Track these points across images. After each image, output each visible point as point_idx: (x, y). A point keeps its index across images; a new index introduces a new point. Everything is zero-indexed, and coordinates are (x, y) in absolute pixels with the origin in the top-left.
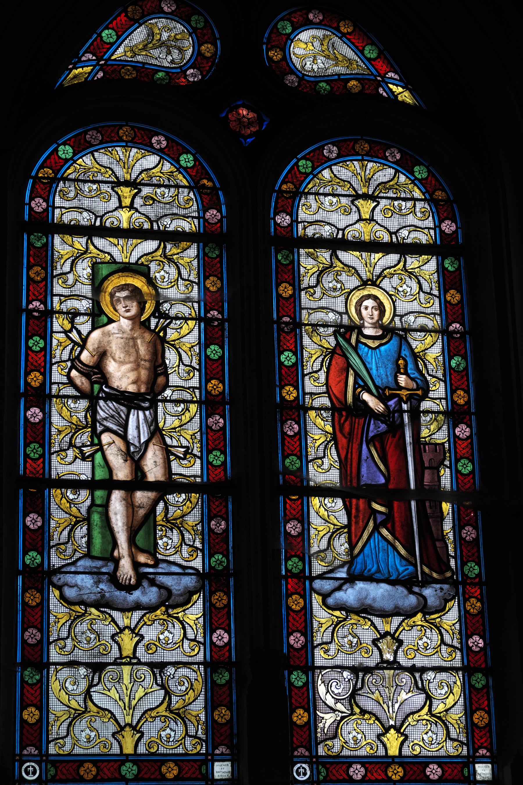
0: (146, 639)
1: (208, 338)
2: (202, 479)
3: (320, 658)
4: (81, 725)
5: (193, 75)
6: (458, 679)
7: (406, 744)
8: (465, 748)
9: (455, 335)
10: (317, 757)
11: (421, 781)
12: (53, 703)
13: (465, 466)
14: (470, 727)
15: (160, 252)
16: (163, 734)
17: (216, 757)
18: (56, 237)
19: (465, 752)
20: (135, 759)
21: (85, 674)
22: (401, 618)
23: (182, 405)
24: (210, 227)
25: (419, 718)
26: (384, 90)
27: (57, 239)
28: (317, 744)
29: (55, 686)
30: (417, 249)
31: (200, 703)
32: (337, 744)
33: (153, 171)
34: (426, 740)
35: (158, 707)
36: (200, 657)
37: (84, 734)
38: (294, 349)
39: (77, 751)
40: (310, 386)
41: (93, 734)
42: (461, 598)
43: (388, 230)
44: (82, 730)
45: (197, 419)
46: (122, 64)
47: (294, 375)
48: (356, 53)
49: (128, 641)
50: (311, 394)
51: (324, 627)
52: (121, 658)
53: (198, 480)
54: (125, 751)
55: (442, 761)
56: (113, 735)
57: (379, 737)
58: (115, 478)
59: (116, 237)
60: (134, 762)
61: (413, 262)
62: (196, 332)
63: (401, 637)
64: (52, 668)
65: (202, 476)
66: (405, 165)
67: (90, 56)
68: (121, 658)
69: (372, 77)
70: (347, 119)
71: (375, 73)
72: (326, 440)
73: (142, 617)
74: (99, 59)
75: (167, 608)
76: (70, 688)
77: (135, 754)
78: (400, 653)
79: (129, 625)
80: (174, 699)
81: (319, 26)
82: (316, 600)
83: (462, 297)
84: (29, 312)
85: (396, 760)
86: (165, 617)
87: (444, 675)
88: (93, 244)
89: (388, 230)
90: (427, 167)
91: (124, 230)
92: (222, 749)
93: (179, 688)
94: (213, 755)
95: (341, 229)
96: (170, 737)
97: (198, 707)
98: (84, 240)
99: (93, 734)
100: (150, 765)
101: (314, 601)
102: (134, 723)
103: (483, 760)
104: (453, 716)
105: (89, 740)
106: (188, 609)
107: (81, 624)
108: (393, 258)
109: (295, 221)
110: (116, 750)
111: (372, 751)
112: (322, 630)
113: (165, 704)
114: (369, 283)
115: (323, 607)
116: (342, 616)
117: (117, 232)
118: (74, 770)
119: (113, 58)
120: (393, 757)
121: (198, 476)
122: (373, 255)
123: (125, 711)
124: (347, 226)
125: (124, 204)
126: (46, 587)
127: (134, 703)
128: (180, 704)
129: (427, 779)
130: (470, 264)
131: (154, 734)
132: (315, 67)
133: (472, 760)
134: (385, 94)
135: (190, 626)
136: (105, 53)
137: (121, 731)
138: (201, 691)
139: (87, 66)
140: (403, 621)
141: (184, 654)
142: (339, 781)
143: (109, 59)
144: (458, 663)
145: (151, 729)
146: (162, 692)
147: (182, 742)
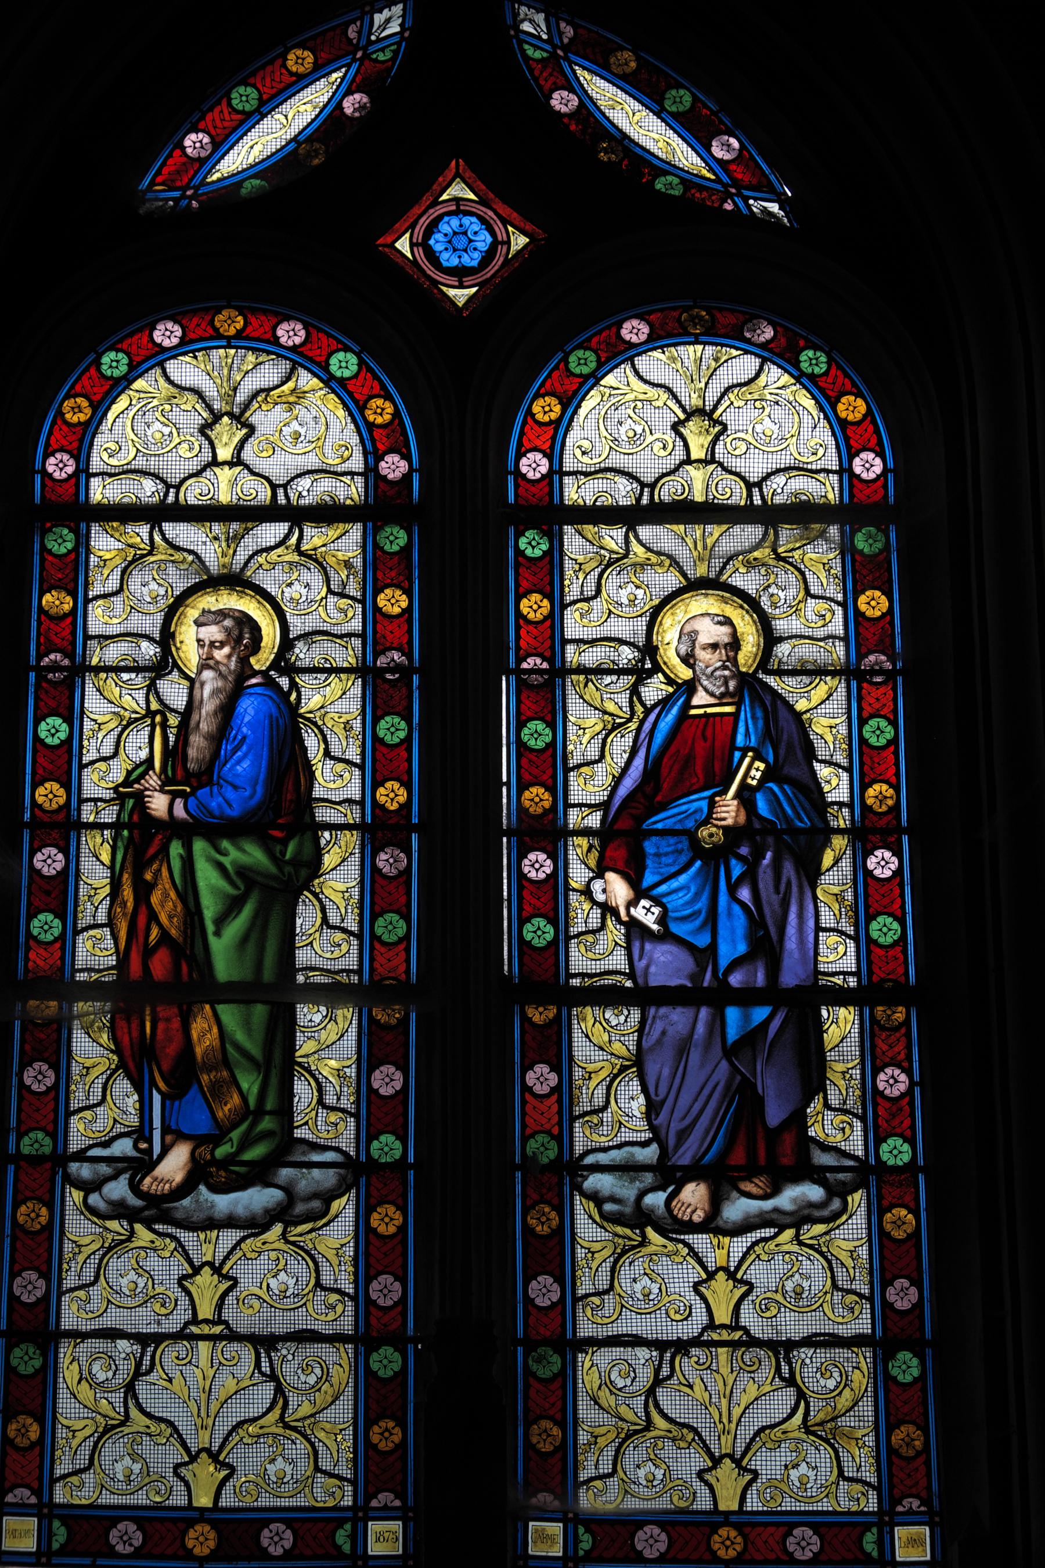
2: (859, 981)
3: (72, 1315)
6: (864, 1358)
7: (229, 1485)
8: (873, 1496)
9: (389, 676)
10: (52, 1505)
11: (174, 1557)
12: (65, 1405)
13: (46, 927)
14: (888, 1458)
16: (794, 1474)
17: (371, 1514)
18: (568, 529)
19: (348, 1501)
22: (239, 1234)
25: (261, 1432)
28: (53, 1481)
29: (69, 1373)
30: (328, 513)
31: (343, 1411)
35: (264, 1414)
39: (107, 1499)
41: (137, 1467)
42: (363, 1191)
43: (743, 479)
49: (722, 1294)
51: (87, 1251)
52: (195, 1321)
54: (722, 1507)
55: (823, 1524)
60: (738, 1527)
61: (314, 537)
66: (782, 353)
68: (195, 1321)
69: (719, 187)
70: (677, 271)
71: (725, 179)
73: (239, 1243)
77: (741, 1511)
78: (746, 1309)
79: (724, 1264)
80: (293, 1400)
84: (40, 670)
85: (207, 1515)
86: (795, 1248)
88: (637, 537)
89: (743, 479)
90: (828, 355)
92: (385, 1498)
93: (822, 1382)
95: (647, 485)
96: (814, 1478)
98: (619, 533)
99: (137, 1467)
100: (238, 1528)
101: (69, 1202)
102: (215, 1447)
105: (128, 1480)
106: (838, 1227)
108: (751, 533)
109: (556, 472)
111: (158, 1499)
112: (81, 1258)
113: (277, 1412)
115: (838, 1222)
118: (778, 1543)
123: (720, 1426)
124: (769, 475)
126: (567, 1189)
127: (214, 1407)
128: (306, 1409)
129: (188, 1555)
130: (922, 537)
131: (778, 1473)
133: (360, 1515)
135: (328, 1260)
137: (714, 1467)
138: (866, 1390)
140: (243, 1239)
142: (766, 1562)
145: (248, 1460)
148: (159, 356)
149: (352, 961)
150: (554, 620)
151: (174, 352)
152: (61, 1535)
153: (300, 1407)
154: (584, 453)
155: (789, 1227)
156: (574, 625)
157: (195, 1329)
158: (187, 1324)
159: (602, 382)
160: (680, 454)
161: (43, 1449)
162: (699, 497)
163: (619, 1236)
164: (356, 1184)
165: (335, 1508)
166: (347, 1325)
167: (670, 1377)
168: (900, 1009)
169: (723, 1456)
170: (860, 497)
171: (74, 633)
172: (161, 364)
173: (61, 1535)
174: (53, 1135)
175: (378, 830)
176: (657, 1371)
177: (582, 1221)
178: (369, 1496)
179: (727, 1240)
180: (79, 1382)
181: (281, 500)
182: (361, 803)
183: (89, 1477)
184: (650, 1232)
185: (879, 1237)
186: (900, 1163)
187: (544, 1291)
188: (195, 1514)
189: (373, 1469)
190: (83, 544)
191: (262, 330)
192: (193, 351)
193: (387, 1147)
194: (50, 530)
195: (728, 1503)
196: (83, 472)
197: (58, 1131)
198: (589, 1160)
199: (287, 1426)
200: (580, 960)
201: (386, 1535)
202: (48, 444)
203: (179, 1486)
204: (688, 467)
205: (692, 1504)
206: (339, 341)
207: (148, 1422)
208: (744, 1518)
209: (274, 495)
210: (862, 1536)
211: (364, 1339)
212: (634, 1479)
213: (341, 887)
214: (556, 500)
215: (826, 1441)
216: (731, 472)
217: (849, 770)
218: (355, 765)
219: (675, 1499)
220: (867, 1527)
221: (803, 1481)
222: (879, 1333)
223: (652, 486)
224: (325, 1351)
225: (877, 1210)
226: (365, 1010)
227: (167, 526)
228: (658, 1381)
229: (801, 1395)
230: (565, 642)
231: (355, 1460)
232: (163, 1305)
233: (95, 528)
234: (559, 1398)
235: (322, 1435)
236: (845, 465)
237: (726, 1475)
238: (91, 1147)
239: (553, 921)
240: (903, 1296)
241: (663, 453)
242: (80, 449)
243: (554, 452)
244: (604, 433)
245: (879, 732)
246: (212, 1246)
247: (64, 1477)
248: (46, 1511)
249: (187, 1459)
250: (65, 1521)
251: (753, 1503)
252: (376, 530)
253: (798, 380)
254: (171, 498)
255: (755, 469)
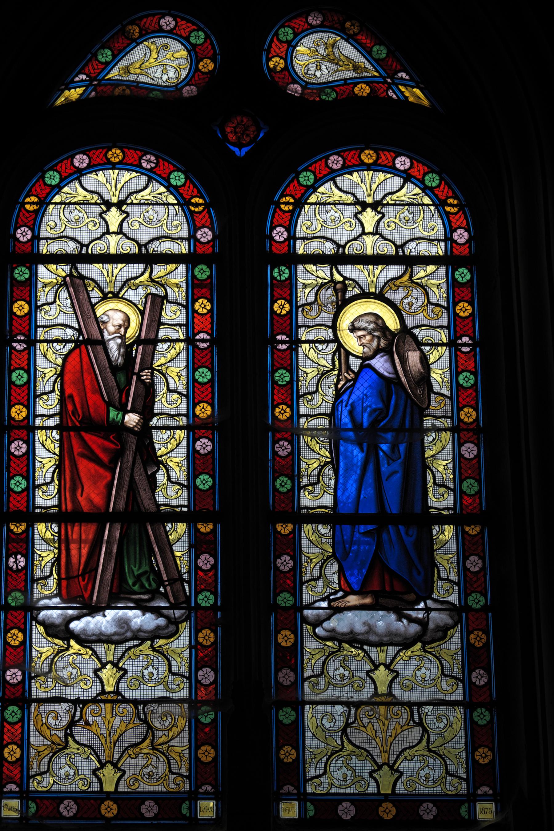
0: (130, 673)
1: (194, 363)
4: (336, 764)
5: (189, 91)
6: (459, 712)
8: (464, 784)
10: (306, 794)
15: (406, 277)
16: (422, 773)
19: (464, 790)
20: (116, 796)
21: (68, 708)
22: (397, 648)
23: (168, 432)
24: (458, 248)
26: (394, 92)
27: (41, 269)
28: (306, 781)
32: (49, 780)
33: (398, 194)
34: (420, 776)
36: (184, 694)
37: (63, 771)
38: (26, 367)
40: (41, 407)
43: (393, 243)
44: (62, 766)
45: (450, 448)
46: (116, 83)
47: (28, 395)
48: (363, 55)
50: (307, 416)
52: (103, 692)
53: (185, 509)
55: (437, 800)
56: (371, 774)
57: (95, 772)
58: (360, 512)
59: (315, 264)
62: (183, 356)
63: (125, 666)
64: (307, 707)
65: (188, 506)
67: (84, 77)
72: (320, 465)
74: (91, 80)
75: (424, 644)
76: (327, 725)
81: (323, 27)
82: (38, 631)
83: (193, 306)
85: (112, 796)
87: (443, 709)
89: (393, 243)
91: (113, 255)
94: (475, 795)
97: (182, 743)
102: (391, 763)
103: (207, 796)
104: (452, 750)
105: (345, 780)
107: (333, 661)
110: (95, 787)
114: (110, 295)
116: (335, 646)
117: (362, 259)
119: (107, 78)
120: (386, 795)
121: (184, 506)
122: (115, 266)
125: (366, 231)
128: (440, 741)
131: (414, 773)
132: (318, 74)
134: (394, 96)
136: (100, 73)
137: (378, 770)
139: (79, 87)
141: (442, 691)
143: (103, 79)
144: (459, 696)
146: (144, 728)
147: (441, 781)
148: (79, 173)
149: (183, 500)
150: (31, 316)
151: (341, 172)
152: (33, 807)
153: (160, 738)
154: (307, 228)
155: (147, 640)
156: (42, 318)
157: (103, 697)
158: (98, 695)
159: (63, 190)
160: (103, 229)
161: (298, 766)
162: (369, 252)
163: (56, 645)
164: (460, 621)
165: (456, 795)
166: (184, 694)
167: (354, 722)
168: (290, 525)
169: (380, 664)
170: (199, 251)
171: (30, 324)
172: (333, 180)
173: (33, 807)
174: (294, 595)
175: (194, 428)
176: (347, 720)
177: (36, 637)
178: (476, 788)
179: (385, 648)
180: (42, 725)
181: (401, 253)
182: (187, 416)
183: (324, 779)
184: (72, 643)
185: (194, 646)
186: (208, 605)
187: (286, 677)
188: (104, 796)
189: (477, 773)
190: (34, 274)
191: (387, 161)
192: (95, 171)
193: (476, 601)
194: (16, 268)
195: (109, 787)
196: (36, 238)
197: (297, 593)
198: (42, 603)
199: (430, 750)
200: (307, 499)
201: (486, 810)
202: (17, 222)
203: (372, 782)
204: (364, 237)
205: (90, 787)
206: (175, 166)
207: (78, 746)
208: (116, 796)
209: (397, 252)
210: (460, 807)
211: (468, 705)
212: (336, 776)
213: (177, 460)
214: (35, 251)
215: (163, 754)
216: (386, 239)
217: (187, 396)
218: (183, 395)
219: (80, 785)
220: (183, 800)
221: (427, 777)
222: (468, 699)
223: (87, 246)
224: (449, 710)
225: (195, 631)
226: (460, 528)
227: (341, 268)
228: (348, 725)
229: (425, 730)
230: (37, 327)
231: (467, 768)
232: (86, 684)
233: (300, 268)
234: (294, 734)
235: (449, 755)
236: (449, 235)
237: (385, 774)
238: (316, 601)
239: (27, 478)
240: (479, 678)
241: (349, 229)
242: (34, 225)
243: (291, 228)
244: (318, 217)
245: (466, 379)
246: (384, 653)
247: (312, 778)
248: (25, 795)
249: (376, 768)
250: (312, 802)
251: (123, 787)
252: (454, 270)
253: (168, 190)
254: (84, 252)
255: (143, 238)
